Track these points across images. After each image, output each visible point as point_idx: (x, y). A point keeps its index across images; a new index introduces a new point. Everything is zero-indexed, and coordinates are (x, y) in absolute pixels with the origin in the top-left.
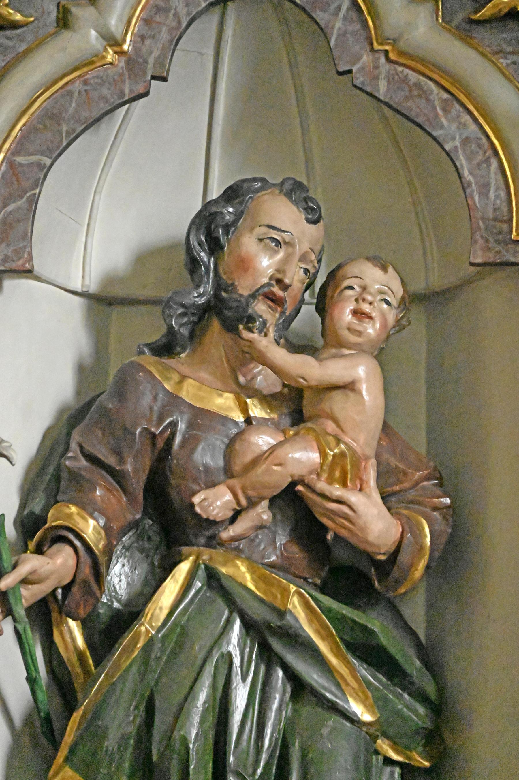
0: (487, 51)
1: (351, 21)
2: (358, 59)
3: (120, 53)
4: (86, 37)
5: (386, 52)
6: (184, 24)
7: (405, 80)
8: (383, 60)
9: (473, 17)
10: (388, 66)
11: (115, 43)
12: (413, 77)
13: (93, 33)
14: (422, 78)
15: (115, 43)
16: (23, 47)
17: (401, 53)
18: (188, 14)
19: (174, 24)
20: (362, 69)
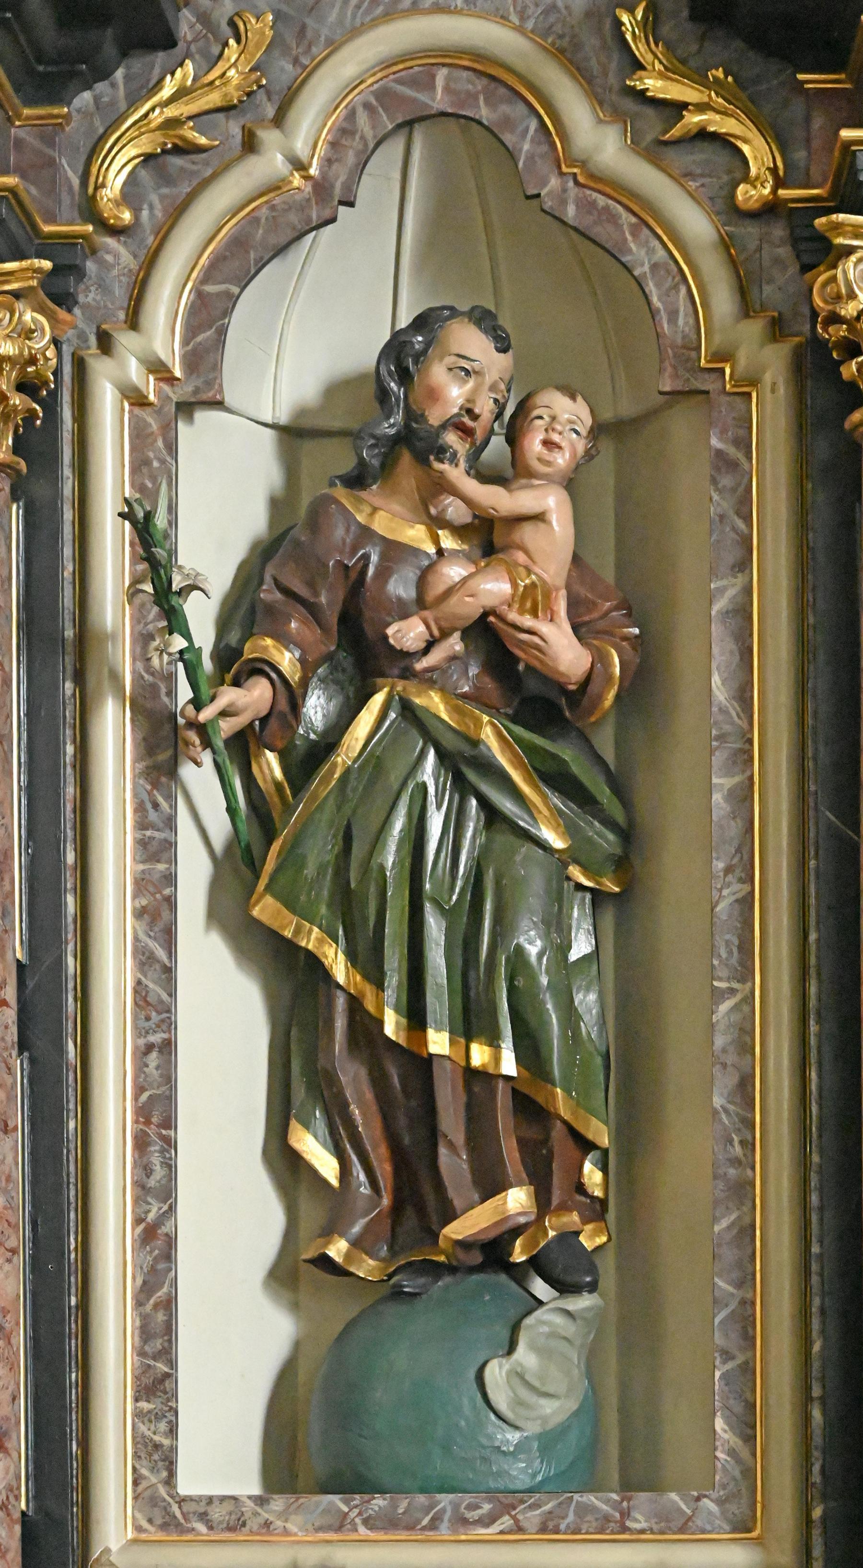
0: (153, 109)
1: (539, 143)
2: (545, 183)
3: (307, 178)
4: (271, 162)
5: (575, 174)
6: (371, 146)
7: (593, 204)
8: (571, 184)
9: (662, 138)
10: (576, 189)
11: (300, 166)
12: (602, 201)
13: (280, 157)
14: (610, 202)
15: (300, 166)
16: (209, 172)
17: (592, 176)
18: (375, 137)
19: (361, 147)
20: (549, 194)
